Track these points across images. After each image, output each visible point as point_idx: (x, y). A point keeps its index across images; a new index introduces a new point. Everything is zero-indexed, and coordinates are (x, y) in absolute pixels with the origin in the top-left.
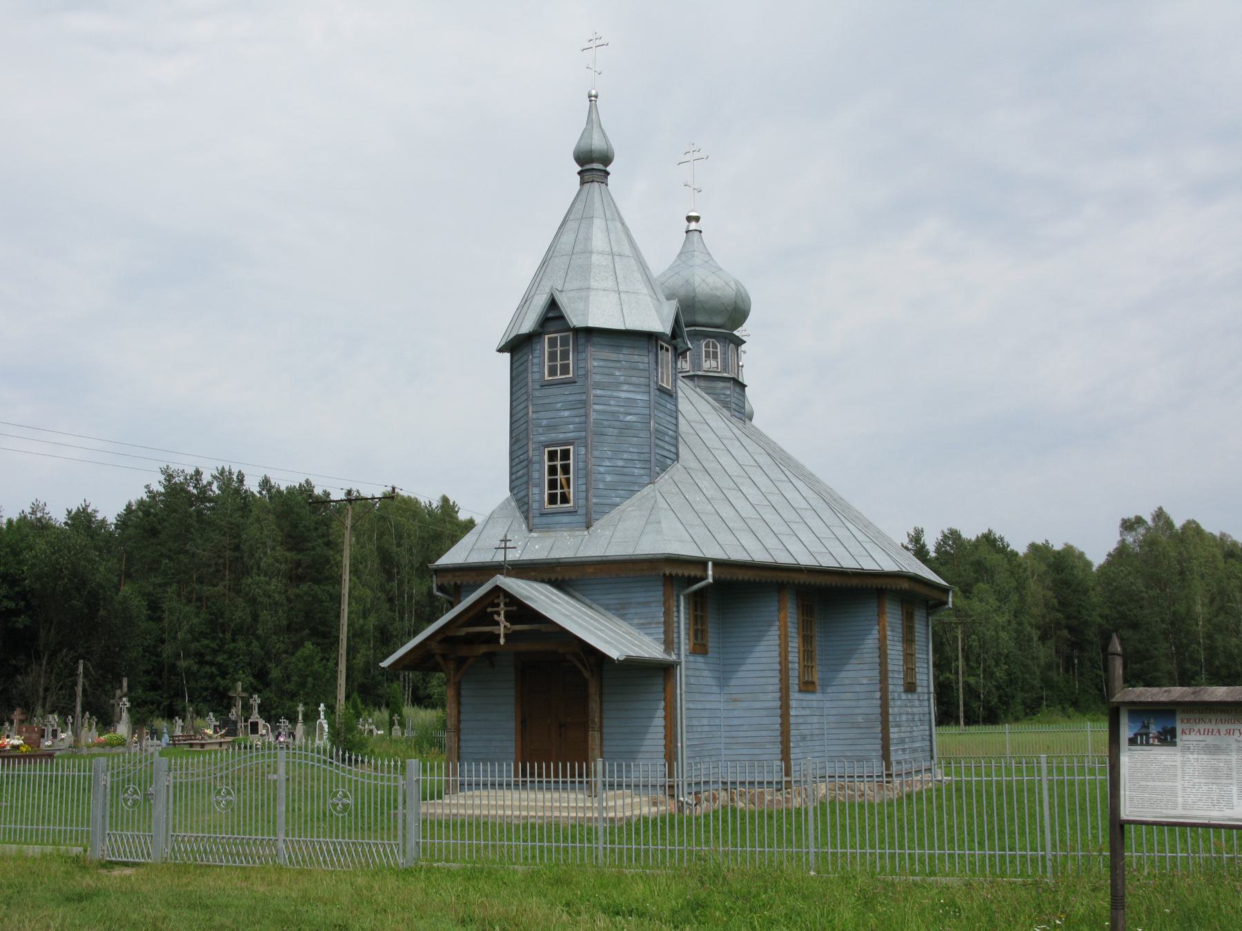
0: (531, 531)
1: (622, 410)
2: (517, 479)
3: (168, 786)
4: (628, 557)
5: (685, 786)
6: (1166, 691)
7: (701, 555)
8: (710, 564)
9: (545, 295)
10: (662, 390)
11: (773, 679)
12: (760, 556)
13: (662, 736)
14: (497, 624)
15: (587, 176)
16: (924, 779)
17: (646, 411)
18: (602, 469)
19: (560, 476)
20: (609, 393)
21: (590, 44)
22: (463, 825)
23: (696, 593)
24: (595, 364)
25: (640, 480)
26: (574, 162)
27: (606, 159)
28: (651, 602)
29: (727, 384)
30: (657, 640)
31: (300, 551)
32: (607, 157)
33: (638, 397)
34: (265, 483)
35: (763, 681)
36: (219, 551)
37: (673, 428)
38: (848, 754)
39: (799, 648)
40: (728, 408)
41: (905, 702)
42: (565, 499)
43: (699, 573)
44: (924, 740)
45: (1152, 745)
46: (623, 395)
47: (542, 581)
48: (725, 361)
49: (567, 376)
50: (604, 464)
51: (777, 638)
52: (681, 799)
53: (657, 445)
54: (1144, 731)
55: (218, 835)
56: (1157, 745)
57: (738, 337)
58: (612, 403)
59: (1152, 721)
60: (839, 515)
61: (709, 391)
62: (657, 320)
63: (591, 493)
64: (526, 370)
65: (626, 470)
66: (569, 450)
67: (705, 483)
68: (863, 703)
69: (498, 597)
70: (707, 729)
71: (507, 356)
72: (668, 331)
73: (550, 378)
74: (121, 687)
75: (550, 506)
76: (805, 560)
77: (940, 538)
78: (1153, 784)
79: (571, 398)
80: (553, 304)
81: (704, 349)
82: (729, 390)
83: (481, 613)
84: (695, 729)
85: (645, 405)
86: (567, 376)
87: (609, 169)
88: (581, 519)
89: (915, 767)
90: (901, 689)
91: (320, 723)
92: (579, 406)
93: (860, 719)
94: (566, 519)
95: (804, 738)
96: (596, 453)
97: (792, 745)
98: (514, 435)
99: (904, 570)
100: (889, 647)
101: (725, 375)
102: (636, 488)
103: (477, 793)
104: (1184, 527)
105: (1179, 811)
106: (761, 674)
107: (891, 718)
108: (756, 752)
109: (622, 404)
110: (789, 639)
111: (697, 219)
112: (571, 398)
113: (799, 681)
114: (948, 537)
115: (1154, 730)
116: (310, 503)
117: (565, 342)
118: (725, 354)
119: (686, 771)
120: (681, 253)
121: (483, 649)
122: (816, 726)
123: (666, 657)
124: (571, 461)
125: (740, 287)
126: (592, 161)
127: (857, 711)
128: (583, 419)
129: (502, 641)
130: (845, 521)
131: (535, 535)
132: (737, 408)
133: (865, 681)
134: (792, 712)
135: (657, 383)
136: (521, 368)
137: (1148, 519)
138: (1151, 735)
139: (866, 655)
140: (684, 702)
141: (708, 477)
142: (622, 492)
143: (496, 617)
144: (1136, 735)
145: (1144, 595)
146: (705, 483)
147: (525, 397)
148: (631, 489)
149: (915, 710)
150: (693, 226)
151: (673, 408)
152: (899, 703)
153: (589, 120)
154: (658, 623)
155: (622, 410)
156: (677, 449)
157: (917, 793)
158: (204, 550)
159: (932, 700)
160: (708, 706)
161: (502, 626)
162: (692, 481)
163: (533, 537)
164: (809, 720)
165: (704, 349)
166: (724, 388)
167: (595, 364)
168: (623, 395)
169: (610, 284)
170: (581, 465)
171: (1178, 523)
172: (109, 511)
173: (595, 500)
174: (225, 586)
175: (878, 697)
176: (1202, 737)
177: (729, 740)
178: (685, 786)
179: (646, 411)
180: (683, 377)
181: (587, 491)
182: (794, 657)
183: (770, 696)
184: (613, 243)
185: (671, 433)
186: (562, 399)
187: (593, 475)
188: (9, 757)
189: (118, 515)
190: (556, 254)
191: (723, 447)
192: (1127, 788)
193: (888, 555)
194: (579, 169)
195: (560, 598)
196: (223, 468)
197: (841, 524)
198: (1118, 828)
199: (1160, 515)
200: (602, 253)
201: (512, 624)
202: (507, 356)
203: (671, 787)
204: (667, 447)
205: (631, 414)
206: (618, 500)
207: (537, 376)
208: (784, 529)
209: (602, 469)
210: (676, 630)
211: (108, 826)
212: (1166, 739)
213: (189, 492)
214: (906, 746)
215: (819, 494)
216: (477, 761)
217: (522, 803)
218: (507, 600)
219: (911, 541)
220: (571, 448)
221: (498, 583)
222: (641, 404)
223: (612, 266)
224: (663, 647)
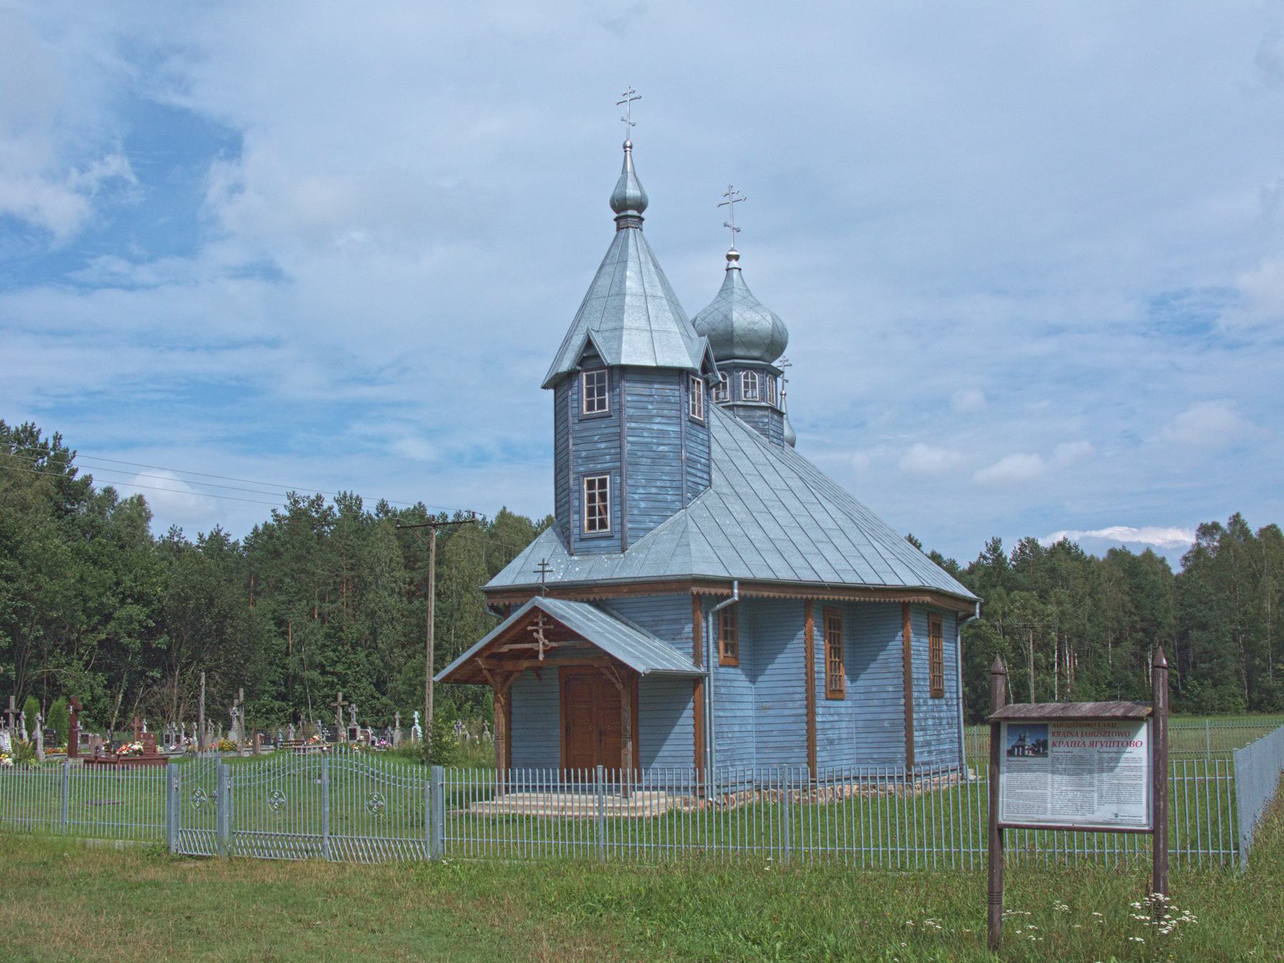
0: (572, 555)
1: (655, 441)
2: (561, 506)
3: (229, 789)
4: (659, 579)
5: (714, 788)
6: (1041, 707)
7: (727, 575)
10: (693, 421)
12: (785, 575)
13: (692, 742)
14: (537, 641)
15: (622, 223)
16: (951, 778)
17: (678, 442)
18: (636, 497)
20: (643, 425)
23: (725, 609)
24: (629, 398)
25: (673, 506)
27: (641, 206)
29: (765, 413)
30: (687, 654)
31: (413, 569)
32: (642, 204)
33: (670, 428)
34: (383, 507)
35: (791, 690)
36: (337, 570)
37: (706, 456)
38: (875, 757)
39: (826, 659)
40: (767, 436)
41: (930, 708)
42: (603, 524)
43: (725, 591)
44: (952, 741)
45: (1028, 756)
46: (656, 427)
47: (582, 601)
48: (763, 391)
50: (638, 492)
51: (803, 650)
52: (711, 799)
53: (689, 473)
54: (1020, 743)
56: (1032, 757)
57: (776, 369)
58: (645, 434)
59: (1027, 734)
60: (866, 534)
61: (748, 419)
62: (685, 356)
63: (627, 518)
64: (567, 405)
65: (660, 497)
66: (606, 479)
67: (736, 507)
68: (888, 709)
69: (537, 617)
70: (738, 734)
71: (551, 392)
72: (698, 366)
74: (238, 698)
76: (829, 577)
77: (1018, 547)
78: (1027, 791)
80: (589, 344)
81: (743, 380)
82: (766, 417)
83: (521, 633)
84: (725, 735)
85: (676, 436)
87: (643, 215)
88: (618, 543)
89: (942, 767)
90: (928, 695)
93: (886, 724)
94: (604, 543)
95: (831, 742)
96: (630, 482)
97: (818, 748)
99: (926, 584)
100: (913, 657)
101: (763, 404)
102: (669, 514)
103: (534, 795)
104: (1263, 532)
105: (1048, 816)
107: (915, 723)
108: (785, 755)
109: (655, 435)
110: (815, 651)
111: (737, 258)
113: (826, 690)
114: (1025, 546)
115: (1029, 742)
116: (398, 528)
118: (763, 384)
119: (714, 771)
120: (721, 290)
121: (526, 664)
122: (845, 731)
123: (695, 669)
124: (608, 490)
125: (778, 322)
126: (627, 209)
127: (884, 716)
128: (618, 450)
130: (872, 540)
131: (576, 558)
132: (775, 435)
133: (890, 689)
134: (819, 719)
135: (688, 414)
136: (564, 403)
137: (1224, 523)
138: (1026, 747)
139: (891, 665)
140: (713, 710)
141: (739, 501)
144: (1013, 747)
145: (1214, 598)
146: (736, 507)
147: (566, 430)
149: (942, 714)
150: (734, 263)
151: (706, 438)
152: (924, 708)
154: (687, 638)
155: (655, 441)
156: (710, 476)
157: (943, 791)
158: (323, 570)
159: (961, 705)
160: (738, 713)
161: (541, 643)
162: (723, 506)
163: (574, 560)
164: (837, 725)
165: (743, 380)
166: (762, 416)
167: (629, 398)
169: (643, 324)
170: (617, 493)
171: (1254, 528)
172: (239, 534)
173: (629, 525)
174: (343, 603)
176: (1070, 749)
177: (760, 745)
178: (714, 788)
179: (678, 442)
180: (723, 407)
181: (622, 517)
182: (820, 668)
183: (798, 704)
184: (646, 286)
185: (703, 461)
186: (599, 432)
187: (628, 502)
188: (105, 763)
189: (246, 538)
190: (593, 296)
191: (756, 473)
192: (1005, 796)
193: (912, 570)
194: (615, 215)
195: (596, 616)
196: (345, 492)
197: (866, 542)
198: (997, 832)
199: (1236, 520)
200: (636, 295)
201: (550, 641)
202: (551, 392)
203: (702, 788)
204: (699, 474)
206: (652, 525)
207: (575, 411)
208: (811, 548)
209: (636, 497)
210: (705, 644)
212: (1039, 750)
213: (310, 516)
214: (933, 748)
215: (849, 516)
216: (527, 766)
217: (582, 805)
218: (545, 619)
219: (989, 550)
220: (608, 477)
223: (644, 306)
224: (693, 660)
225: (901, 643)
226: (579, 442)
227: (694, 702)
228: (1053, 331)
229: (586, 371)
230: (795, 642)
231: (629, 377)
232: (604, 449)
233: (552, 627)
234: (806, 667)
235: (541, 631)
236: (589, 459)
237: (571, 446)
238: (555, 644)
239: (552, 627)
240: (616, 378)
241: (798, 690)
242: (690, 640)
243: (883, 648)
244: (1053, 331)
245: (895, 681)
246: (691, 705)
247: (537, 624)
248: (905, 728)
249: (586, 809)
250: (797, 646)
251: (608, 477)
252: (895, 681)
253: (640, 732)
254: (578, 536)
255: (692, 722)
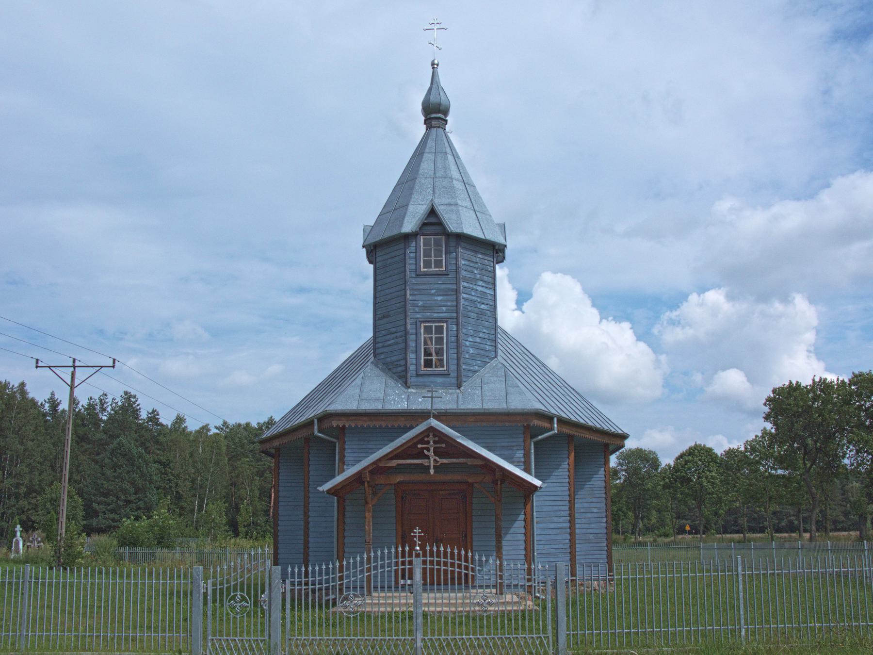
0: (409, 387)
8: (555, 419)
9: (425, 206)
11: (564, 507)
13: (523, 547)
14: (427, 457)
19: (433, 348)
20: (471, 286)
21: (432, 27)
22: (474, 619)
24: (463, 262)
26: (420, 107)
28: (513, 446)
35: (556, 508)
46: (479, 289)
49: (441, 269)
50: (469, 340)
51: (567, 477)
55: (401, 637)
58: (473, 293)
63: (462, 360)
65: (482, 346)
66: (443, 326)
68: (593, 525)
73: (425, 270)
75: (425, 369)
79: (443, 286)
80: (432, 212)
86: (441, 269)
87: (447, 118)
88: (454, 380)
91: (17, 540)
92: (453, 293)
93: (591, 537)
94: (439, 380)
96: (464, 331)
98: (378, 313)
102: (488, 361)
106: (554, 503)
109: (479, 295)
112: (443, 286)
117: (438, 244)
126: (432, 113)
127: (589, 531)
129: (432, 472)
133: (595, 510)
139: (596, 492)
142: (479, 362)
143: (426, 452)
148: (484, 360)
153: (432, 83)
155: (479, 300)
161: (432, 460)
167: (463, 262)
168: (479, 289)
170: (453, 339)
175: (604, 521)
183: (562, 519)
186: (436, 286)
205: (484, 304)
209: (467, 343)
211: (210, 631)
218: (437, 439)
220: (445, 325)
221: (432, 424)
222: (490, 297)
225: (603, 476)
226: (416, 293)
227: (525, 514)
228: (302, 290)
229: (423, 235)
230: (560, 470)
231: (462, 244)
232: (441, 301)
233: (444, 445)
234: (569, 490)
235: (432, 449)
236: (425, 308)
237: (408, 296)
238: (445, 461)
239: (444, 445)
240: (453, 244)
241: (563, 508)
242: (521, 464)
243: (589, 479)
244: (302, 290)
245: (598, 505)
246: (522, 517)
247: (428, 443)
248: (607, 539)
249: (455, 605)
250: (561, 474)
251: (445, 325)
252: (598, 505)
253: (474, 540)
254: (415, 373)
255: (523, 531)
